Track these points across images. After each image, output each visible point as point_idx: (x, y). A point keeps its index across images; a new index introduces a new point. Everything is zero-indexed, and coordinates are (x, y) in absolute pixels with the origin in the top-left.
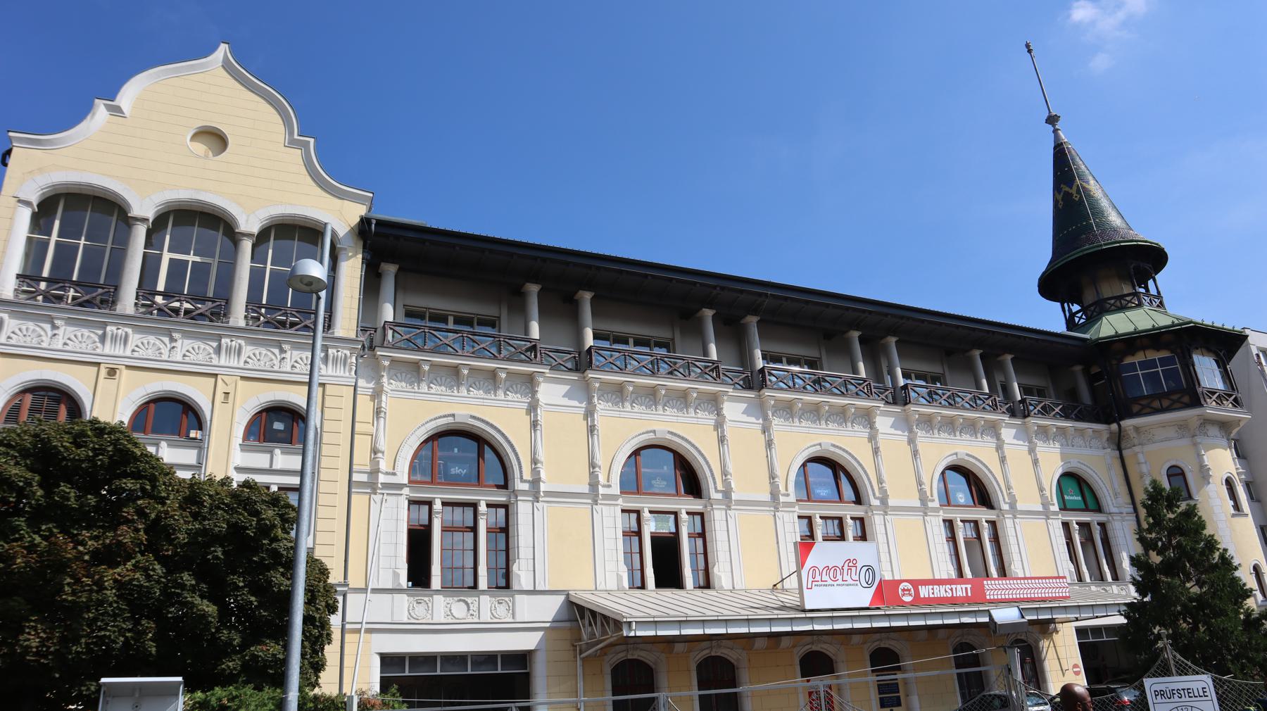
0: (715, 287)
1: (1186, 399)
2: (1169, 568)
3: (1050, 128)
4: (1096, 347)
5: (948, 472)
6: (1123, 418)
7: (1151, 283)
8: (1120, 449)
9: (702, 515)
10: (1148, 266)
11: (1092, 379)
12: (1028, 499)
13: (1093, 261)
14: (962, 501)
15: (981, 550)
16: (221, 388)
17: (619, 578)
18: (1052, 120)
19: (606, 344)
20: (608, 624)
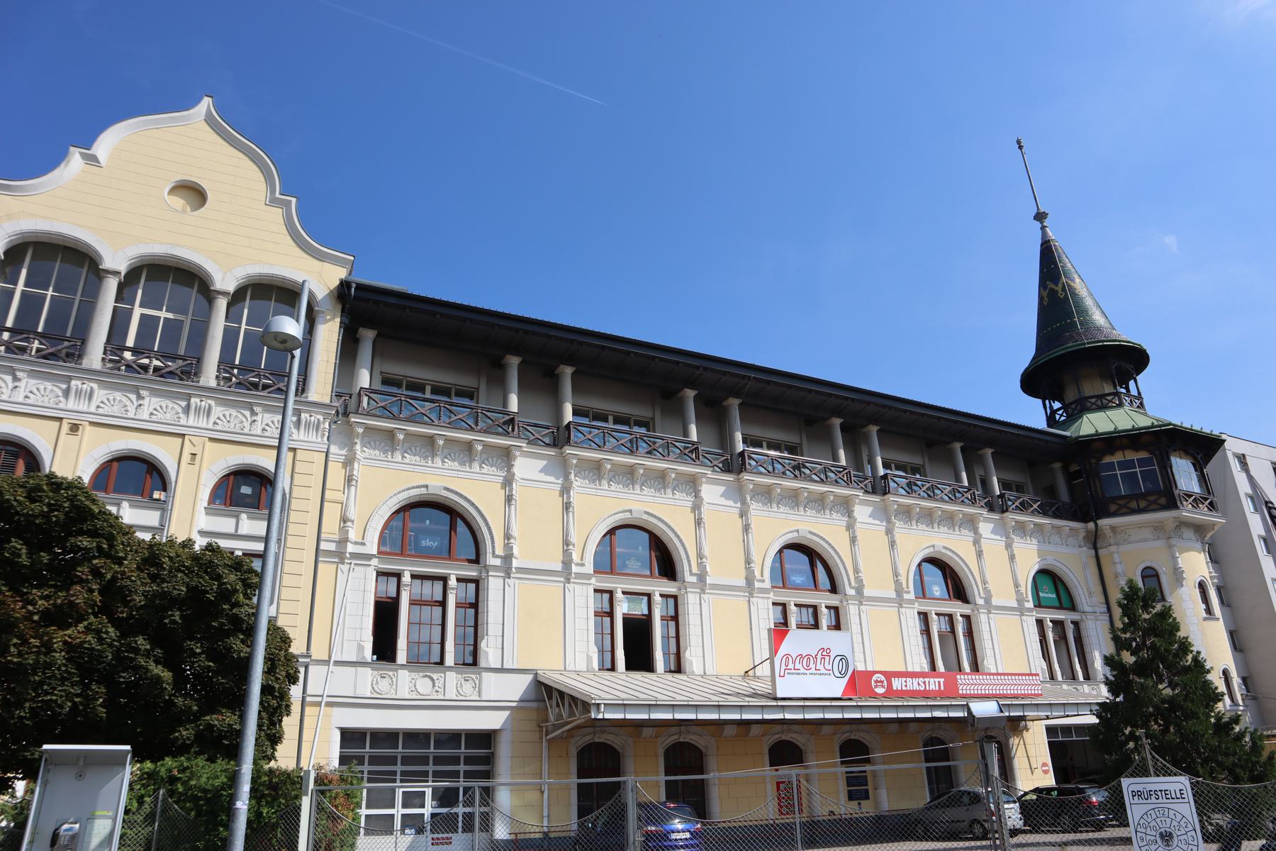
0: (698, 367)
1: (1163, 501)
3: (1038, 225)
4: (1079, 444)
5: (924, 564)
7: (1132, 383)
8: (1096, 548)
10: (1130, 367)
11: (1070, 477)
12: (1004, 595)
13: (1076, 359)
14: (937, 594)
15: (955, 643)
17: (589, 658)
18: (1040, 217)
19: (585, 421)
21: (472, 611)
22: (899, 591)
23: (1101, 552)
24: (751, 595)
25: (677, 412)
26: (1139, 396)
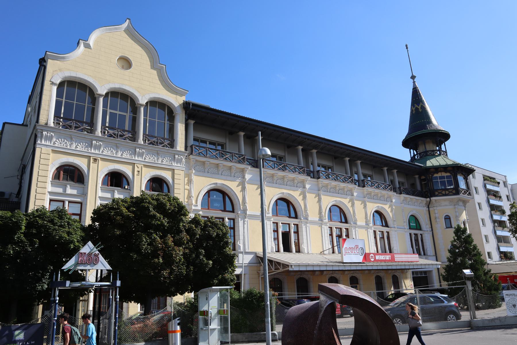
0: (306, 139)
1: (454, 192)
3: (412, 81)
4: (423, 169)
5: (278, 201)
6: (432, 197)
7: (443, 146)
8: (428, 207)
9: (234, 220)
10: (443, 140)
11: (421, 181)
12: (361, 222)
13: (423, 134)
15: (386, 244)
16: (136, 169)
17: (272, 247)
18: (413, 77)
20: (272, 265)
21: (232, 230)
22: (321, 219)
23: (430, 209)
24: (322, 224)
26: (446, 152)
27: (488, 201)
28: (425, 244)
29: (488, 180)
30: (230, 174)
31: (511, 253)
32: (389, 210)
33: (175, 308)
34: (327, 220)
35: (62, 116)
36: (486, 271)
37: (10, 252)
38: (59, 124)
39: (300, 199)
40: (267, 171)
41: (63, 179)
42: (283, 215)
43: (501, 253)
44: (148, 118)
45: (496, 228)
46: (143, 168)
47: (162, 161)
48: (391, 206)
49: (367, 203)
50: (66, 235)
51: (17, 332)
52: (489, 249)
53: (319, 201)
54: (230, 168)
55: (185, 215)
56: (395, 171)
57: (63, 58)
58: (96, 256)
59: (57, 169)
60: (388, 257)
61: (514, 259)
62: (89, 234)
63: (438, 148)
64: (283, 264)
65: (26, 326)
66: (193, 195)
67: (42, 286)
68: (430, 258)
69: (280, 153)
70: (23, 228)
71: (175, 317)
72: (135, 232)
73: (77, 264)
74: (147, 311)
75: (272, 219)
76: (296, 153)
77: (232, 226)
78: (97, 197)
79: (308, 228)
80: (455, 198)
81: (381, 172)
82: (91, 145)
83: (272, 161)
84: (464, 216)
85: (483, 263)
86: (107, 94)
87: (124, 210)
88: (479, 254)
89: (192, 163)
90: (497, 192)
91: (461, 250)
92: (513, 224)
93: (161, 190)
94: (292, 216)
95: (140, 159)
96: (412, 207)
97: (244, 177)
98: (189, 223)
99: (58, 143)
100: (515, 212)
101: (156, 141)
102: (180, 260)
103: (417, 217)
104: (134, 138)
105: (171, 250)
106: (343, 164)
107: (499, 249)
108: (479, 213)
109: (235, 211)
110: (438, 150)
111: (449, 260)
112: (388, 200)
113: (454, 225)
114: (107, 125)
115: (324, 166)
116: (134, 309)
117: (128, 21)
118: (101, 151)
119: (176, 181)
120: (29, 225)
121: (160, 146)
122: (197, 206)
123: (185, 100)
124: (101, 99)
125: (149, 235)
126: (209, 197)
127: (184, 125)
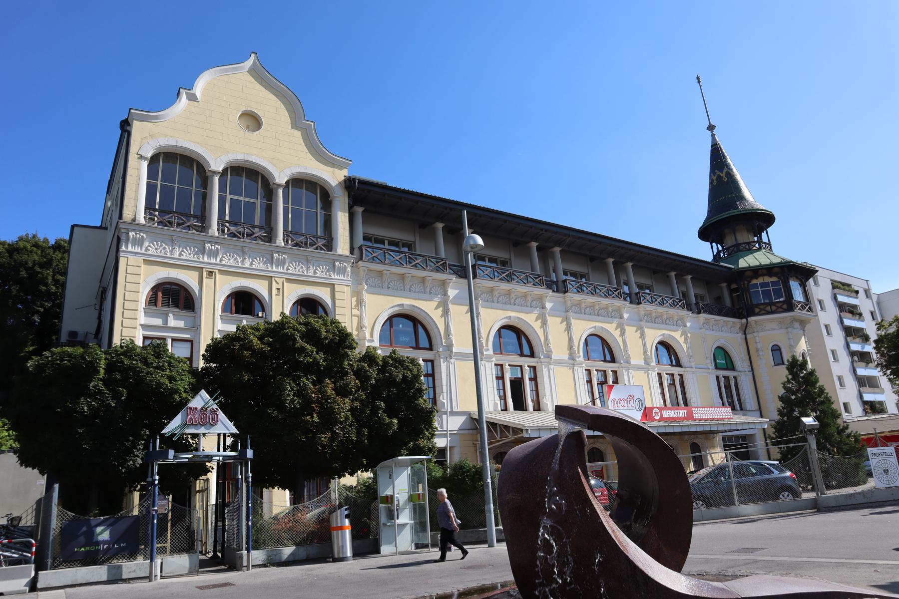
1: (785, 306)
2: (800, 403)
3: (709, 133)
4: (734, 271)
5: (502, 330)
6: (750, 316)
7: (764, 235)
8: (745, 334)
9: (432, 361)
10: (764, 225)
11: (731, 291)
12: (637, 359)
15: (678, 392)
16: (274, 286)
17: (495, 404)
18: (711, 128)
19: (370, 244)
20: (509, 432)
22: (572, 357)
23: (748, 336)
24: (574, 365)
25: (431, 236)
26: (769, 244)
27: (842, 322)
28: (741, 392)
29: (839, 288)
30: (423, 289)
31: (881, 403)
32: (681, 340)
33: (340, 495)
34: (582, 359)
35: (157, 207)
36: (841, 427)
37: (83, 408)
38: (154, 220)
39: (537, 326)
40: (482, 284)
41: (163, 304)
42: (510, 353)
43: (865, 403)
44: (290, 206)
45: (855, 364)
46: (285, 284)
47: (315, 272)
48: (684, 334)
49: (646, 330)
50: (166, 382)
51: (99, 529)
52: (846, 396)
53: (568, 328)
54: (423, 280)
55: (351, 347)
56: (689, 277)
57: (156, 117)
58: (214, 412)
59: (153, 289)
60: (682, 413)
61: (886, 412)
62: (201, 380)
63: (756, 239)
64: (513, 428)
65: (112, 520)
66: (366, 324)
67: (134, 461)
68: (749, 413)
69: (501, 254)
70: (102, 371)
71: (340, 506)
72: (274, 377)
73: (185, 425)
74: (296, 499)
75: (494, 359)
76: (527, 254)
77: (430, 372)
78: (216, 330)
79: (551, 372)
80: (787, 317)
81: (667, 281)
82: (203, 251)
83: (490, 267)
84: (803, 346)
85: (836, 415)
86: (225, 171)
87: (256, 341)
88: (828, 401)
89: (362, 273)
90: (855, 307)
91: (799, 395)
92: (883, 355)
93: (315, 312)
94: (525, 353)
95: (280, 269)
96: (719, 334)
97: (445, 294)
98: (359, 361)
99: (153, 249)
100: (885, 335)
101: (304, 241)
102: (346, 419)
103: (727, 349)
104: (269, 237)
105: (331, 403)
106: (604, 268)
107: (861, 397)
108: (827, 339)
109: (434, 347)
110: (757, 242)
111: (781, 413)
112: (679, 323)
113: (787, 357)
114: (227, 218)
115: (574, 274)
116: (279, 500)
117: (253, 56)
118: (219, 259)
119: (337, 303)
120: (111, 368)
121: (311, 249)
122: (373, 341)
123: (347, 175)
124: (216, 179)
125: (296, 379)
126: (391, 326)
127: (347, 215)
